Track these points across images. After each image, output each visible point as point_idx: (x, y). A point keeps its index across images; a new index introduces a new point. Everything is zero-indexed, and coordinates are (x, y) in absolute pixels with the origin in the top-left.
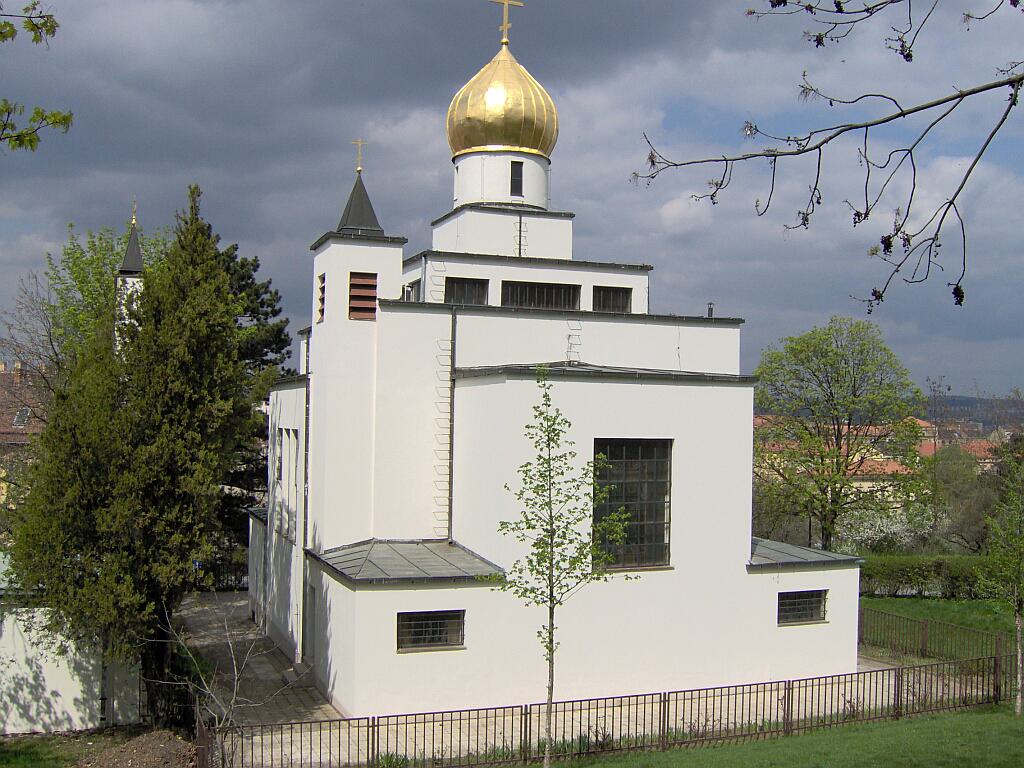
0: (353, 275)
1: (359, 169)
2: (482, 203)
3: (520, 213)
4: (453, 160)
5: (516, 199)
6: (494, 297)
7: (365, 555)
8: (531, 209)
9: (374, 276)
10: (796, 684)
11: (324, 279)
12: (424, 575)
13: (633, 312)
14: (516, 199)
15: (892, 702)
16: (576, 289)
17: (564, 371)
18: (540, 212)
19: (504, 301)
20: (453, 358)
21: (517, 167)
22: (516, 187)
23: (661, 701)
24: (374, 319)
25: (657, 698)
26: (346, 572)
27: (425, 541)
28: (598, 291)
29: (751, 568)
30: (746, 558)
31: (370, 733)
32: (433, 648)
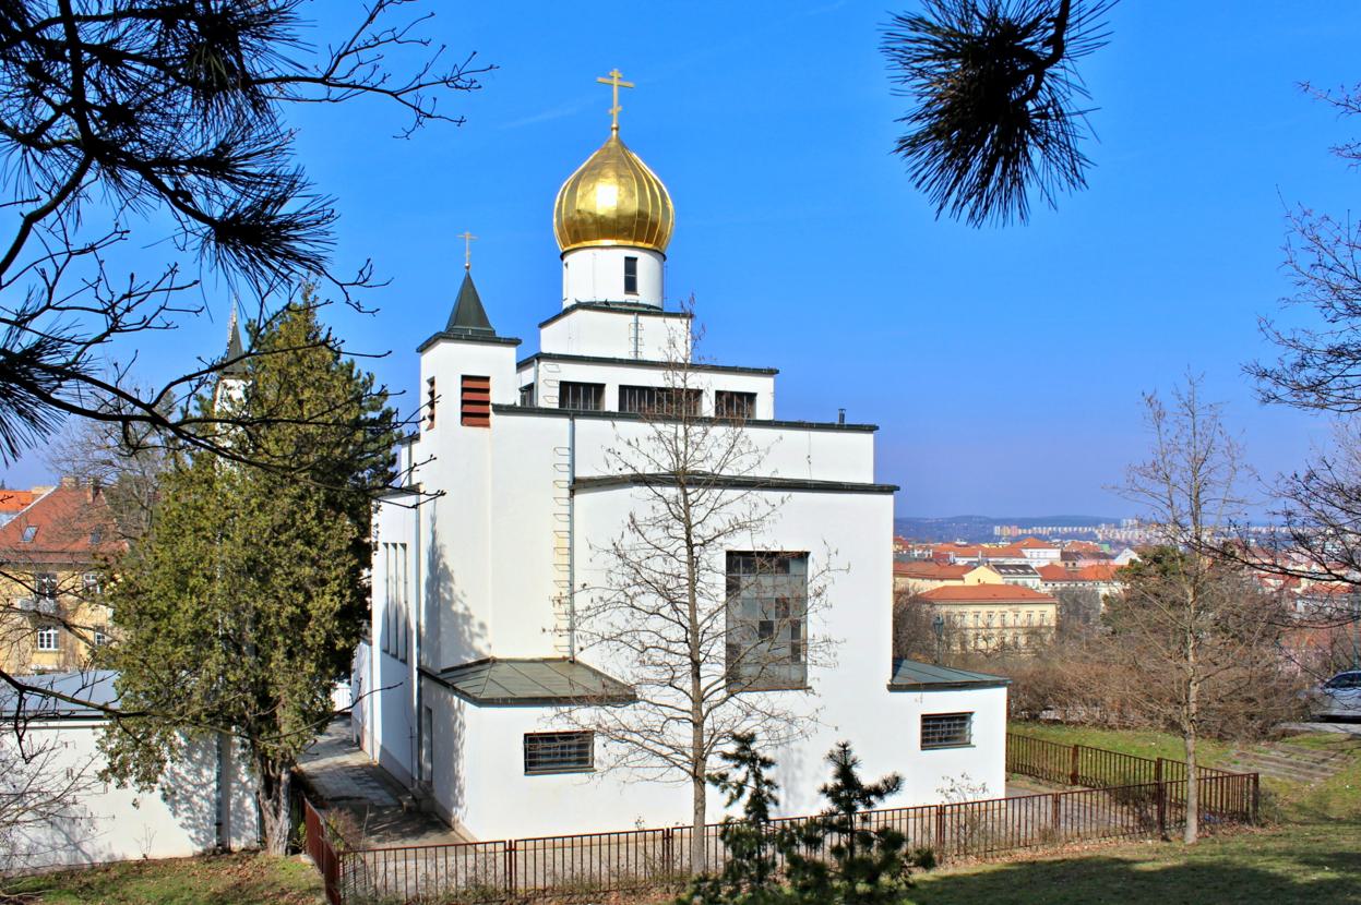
0: (465, 378)
5: (631, 298)
6: (611, 402)
9: (487, 379)
16: (599, 389)
20: (572, 466)
21: (630, 263)
22: (631, 285)
24: (487, 425)
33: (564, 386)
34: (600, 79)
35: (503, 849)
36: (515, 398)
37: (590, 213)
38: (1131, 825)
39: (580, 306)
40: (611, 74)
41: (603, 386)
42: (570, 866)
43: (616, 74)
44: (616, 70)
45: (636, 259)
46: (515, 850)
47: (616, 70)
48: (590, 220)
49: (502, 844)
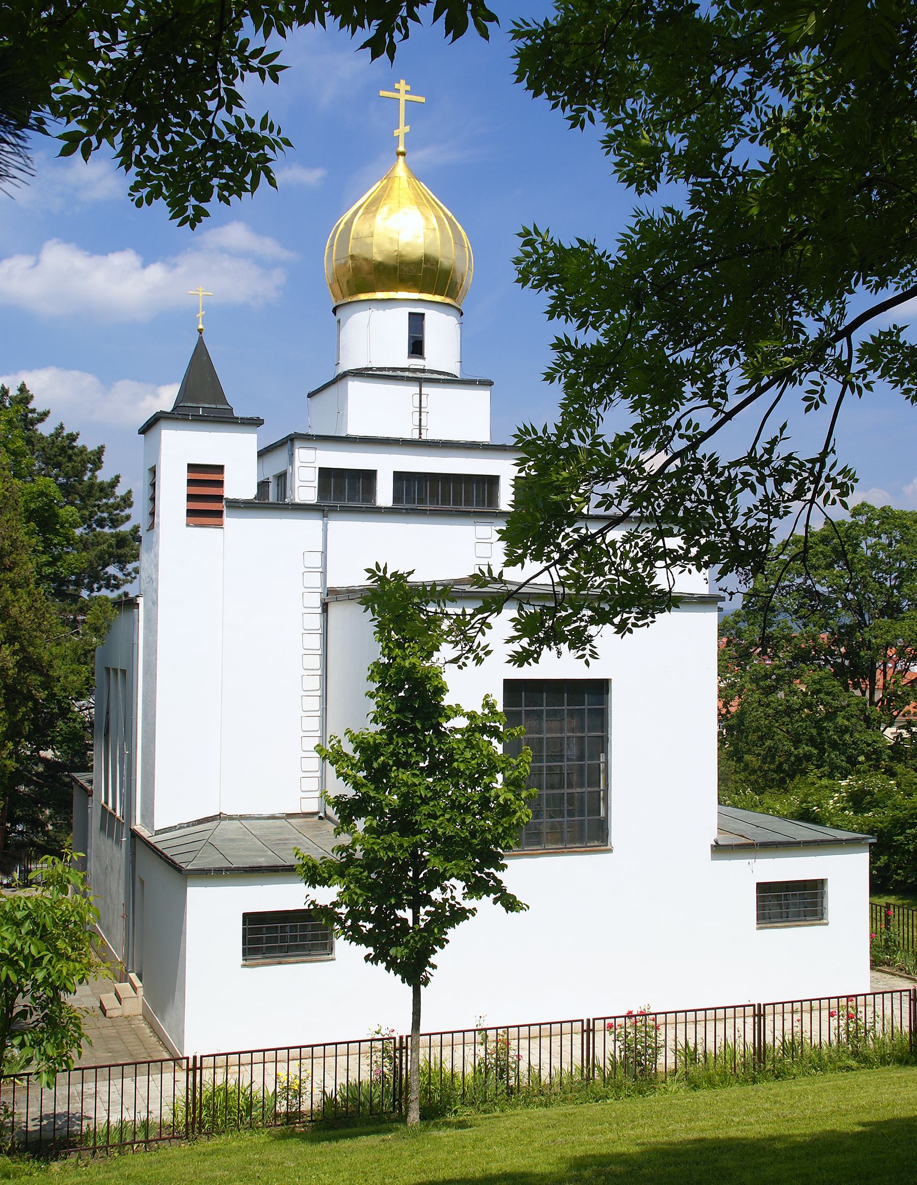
0: (192, 468)
1: (201, 327)
2: (371, 369)
3: (420, 382)
4: (335, 311)
5: (416, 363)
6: (384, 495)
7: (206, 835)
8: (442, 377)
9: (220, 469)
10: (769, 1009)
11: (155, 472)
12: (225, 864)
13: (297, 501)
14: (416, 363)
15: (577, 1061)
16: (369, 476)
17: (464, 592)
18: (450, 380)
19: (397, 498)
20: (324, 573)
21: (416, 322)
22: (416, 348)
23: (583, 1031)
24: (220, 526)
25: (750, 1011)
26: (177, 860)
27: (290, 816)
28: (400, 477)
29: (719, 850)
30: (711, 834)
31: (191, 1079)
32: (314, 958)
33: (325, 474)
34: (382, 93)
35: (204, 1071)
36: (250, 493)
37: (366, 260)
38: (524, 1043)
39: (362, 374)
40: (397, 86)
41: (374, 473)
42: (790, 1032)
43: (402, 86)
44: (403, 82)
45: (422, 315)
46: (593, 1030)
47: (403, 82)
48: (366, 268)
49: (907, 993)
